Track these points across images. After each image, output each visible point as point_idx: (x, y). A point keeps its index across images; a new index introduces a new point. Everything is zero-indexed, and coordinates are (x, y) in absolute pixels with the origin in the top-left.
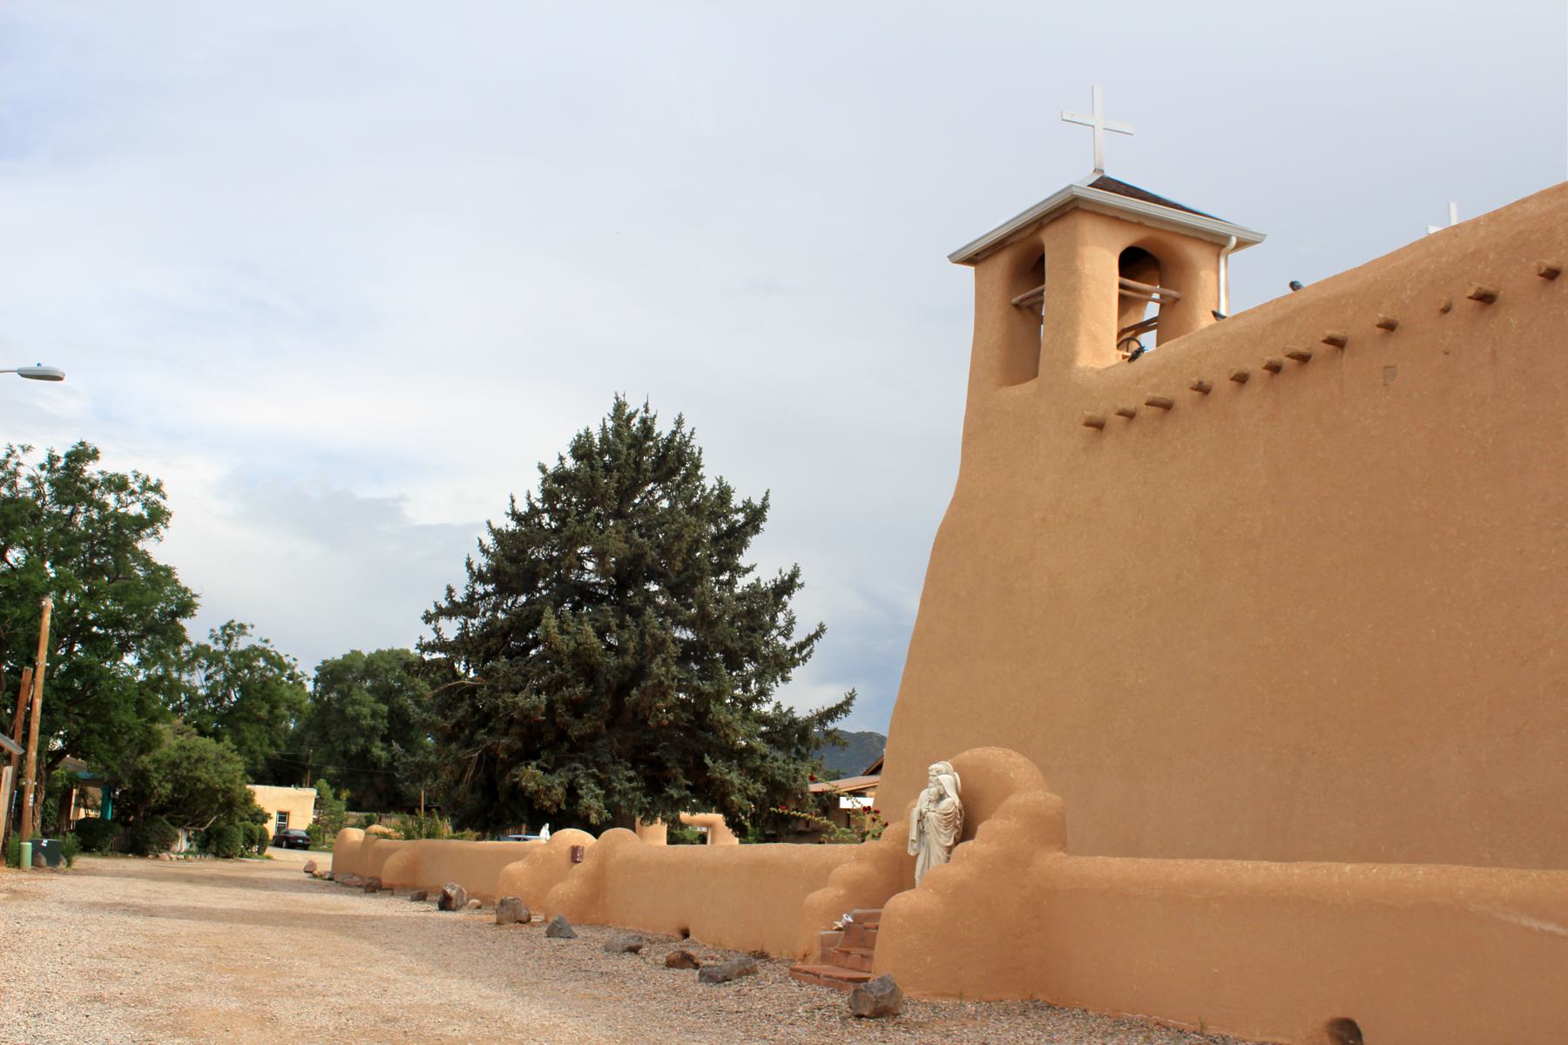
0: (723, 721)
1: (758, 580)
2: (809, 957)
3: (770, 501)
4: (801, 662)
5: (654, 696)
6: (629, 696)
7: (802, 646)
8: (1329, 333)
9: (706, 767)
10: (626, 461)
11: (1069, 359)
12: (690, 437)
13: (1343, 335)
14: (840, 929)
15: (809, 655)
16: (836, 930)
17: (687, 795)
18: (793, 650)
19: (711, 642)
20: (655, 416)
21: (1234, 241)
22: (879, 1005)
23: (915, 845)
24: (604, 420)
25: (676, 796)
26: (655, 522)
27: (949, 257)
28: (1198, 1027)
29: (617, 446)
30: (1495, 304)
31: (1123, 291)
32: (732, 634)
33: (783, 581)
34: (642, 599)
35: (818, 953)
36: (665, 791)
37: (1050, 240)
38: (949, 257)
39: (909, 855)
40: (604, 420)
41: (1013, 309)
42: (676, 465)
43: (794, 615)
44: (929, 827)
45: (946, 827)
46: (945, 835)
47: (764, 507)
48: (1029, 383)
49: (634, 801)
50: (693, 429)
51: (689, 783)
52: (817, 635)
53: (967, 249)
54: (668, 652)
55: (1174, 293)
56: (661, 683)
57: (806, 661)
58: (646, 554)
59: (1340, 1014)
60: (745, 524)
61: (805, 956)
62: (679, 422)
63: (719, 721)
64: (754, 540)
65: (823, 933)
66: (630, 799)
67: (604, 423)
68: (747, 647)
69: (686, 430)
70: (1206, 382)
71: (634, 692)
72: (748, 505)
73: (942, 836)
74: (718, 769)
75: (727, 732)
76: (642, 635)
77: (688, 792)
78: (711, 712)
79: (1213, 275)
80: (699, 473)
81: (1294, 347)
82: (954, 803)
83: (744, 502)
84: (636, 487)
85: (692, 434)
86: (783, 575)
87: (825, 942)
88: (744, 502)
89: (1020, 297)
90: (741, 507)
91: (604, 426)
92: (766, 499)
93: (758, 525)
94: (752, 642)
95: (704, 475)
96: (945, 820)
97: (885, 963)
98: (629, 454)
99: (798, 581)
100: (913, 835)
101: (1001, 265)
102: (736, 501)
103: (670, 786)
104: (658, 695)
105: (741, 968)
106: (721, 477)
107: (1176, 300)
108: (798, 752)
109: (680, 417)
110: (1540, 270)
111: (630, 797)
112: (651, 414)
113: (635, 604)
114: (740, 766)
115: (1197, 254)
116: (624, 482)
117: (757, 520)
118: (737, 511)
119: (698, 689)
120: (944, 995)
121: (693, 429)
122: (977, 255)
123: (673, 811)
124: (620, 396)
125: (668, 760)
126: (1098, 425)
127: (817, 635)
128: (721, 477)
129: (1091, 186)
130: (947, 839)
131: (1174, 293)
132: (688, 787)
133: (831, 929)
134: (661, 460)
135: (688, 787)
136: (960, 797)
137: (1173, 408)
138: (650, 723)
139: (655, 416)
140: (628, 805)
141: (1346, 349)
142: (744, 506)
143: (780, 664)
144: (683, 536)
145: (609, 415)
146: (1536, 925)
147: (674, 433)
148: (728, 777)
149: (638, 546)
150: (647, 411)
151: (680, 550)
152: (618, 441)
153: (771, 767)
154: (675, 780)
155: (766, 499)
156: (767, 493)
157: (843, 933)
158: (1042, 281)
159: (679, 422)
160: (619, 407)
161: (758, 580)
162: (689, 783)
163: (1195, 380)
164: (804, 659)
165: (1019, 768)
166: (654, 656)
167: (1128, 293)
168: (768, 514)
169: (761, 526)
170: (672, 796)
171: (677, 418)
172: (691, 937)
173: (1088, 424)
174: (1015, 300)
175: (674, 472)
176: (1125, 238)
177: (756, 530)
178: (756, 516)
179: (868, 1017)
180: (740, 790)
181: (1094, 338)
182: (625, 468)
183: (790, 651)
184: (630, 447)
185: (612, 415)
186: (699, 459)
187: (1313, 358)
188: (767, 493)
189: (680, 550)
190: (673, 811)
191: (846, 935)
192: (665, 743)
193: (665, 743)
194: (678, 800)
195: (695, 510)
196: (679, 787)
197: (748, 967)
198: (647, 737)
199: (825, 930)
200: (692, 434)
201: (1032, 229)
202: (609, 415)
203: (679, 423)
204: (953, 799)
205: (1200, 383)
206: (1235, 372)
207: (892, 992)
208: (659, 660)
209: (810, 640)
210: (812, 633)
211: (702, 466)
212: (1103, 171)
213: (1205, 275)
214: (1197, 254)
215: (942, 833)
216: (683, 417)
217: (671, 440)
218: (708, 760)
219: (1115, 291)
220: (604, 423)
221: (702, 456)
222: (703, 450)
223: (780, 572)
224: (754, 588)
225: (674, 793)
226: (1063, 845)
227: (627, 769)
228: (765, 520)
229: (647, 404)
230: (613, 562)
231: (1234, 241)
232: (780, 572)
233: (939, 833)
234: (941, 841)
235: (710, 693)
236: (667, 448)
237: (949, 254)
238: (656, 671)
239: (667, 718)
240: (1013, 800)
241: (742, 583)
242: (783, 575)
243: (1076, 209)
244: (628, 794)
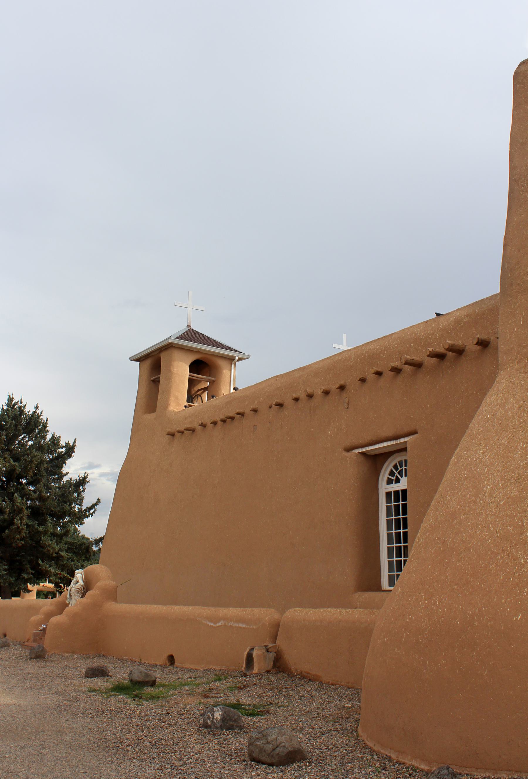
0: (47, 544)
1: (71, 479)
2: (29, 640)
3: (76, 444)
4: (90, 516)
5: (15, 533)
6: (5, 533)
7: (89, 509)
8: (238, 411)
9: (39, 565)
10: (10, 426)
11: (166, 406)
12: (41, 415)
13: (243, 411)
14: (41, 630)
15: (94, 512)
16: (40, 630)
17: (31, 577)
18: (85, 510)
19: (44, 509)
20: (26, 405)
21: (237, 358)
22: (37, 654)
23: (69, 600)
24: (3, 405)
25: (26, 577)
26: (22, 453)
27: (129, 358)
28: (139, 660)
29: (6, 419)
30: (283, 407)
31: (190, 377)
32: (54, 504)
33: (80, 480)
34: (15, 489)
35: (32, 639)
36: (22, 575)
37: (164, 356)
38: (129, 358)
39: (66, 603)
40: (3, 405)
41: (151, 382)
42: (34, 427)
43: (83, 496)
44: (72, 593)
45: (78, 593)
46: (77, 596)
47: (74, 446)
48: (152, 414)
49: (7, 580)
50: (42, 411)
51: (33, 572)
52: (97, 504)
53: (138, 355)
54: (24, 514)
55: (212, 379)
56: (18, 527)
57: (93, 515)
58: (16, 469)
59: (170, 654)
60: (65, 454)
61: (28, 640)
62: (37, 408)
63: (45, 544)
64: (68, 461)
65: (34, 631)
66: (5, 579)
67: (3, 407)
68: (61, 510)
69: (39, 412)
70: (204, 423)
71: (7, 531)
72: (68, 445)
73: (76, 596)
74: (44, 565)
75: (49, 549)
76: (13, 506)
77: (32, 576)
78: (42, 540)
79: (229, 372)
80: (47, 429)
81: (228, 414)
82: (81, 584)
83: (66, 443)
84: (16, 437)
85: (41, 413)
86: (80, 477)
87: (35, 635)
88: (66, 443)
89: (154, 378)
90: (65, 445)
91: (3, 408)
92: (74, 443)
93: (71, 454)
94: (63, 508)
95: (49, 430)
96: (77, 590)
97: (47, 642)
98: (12, 423)
99: (87, 480)
100: (68, 596)
101: (148, 363)
102: (63, 443)
103: (24, 573)
104: (17, 532)
105: (3, 644)
106: (54, 433)
107: (214, 381)
108: (86, 557)
109: (37, 405)
110: (292, 398)
111: (5, 578)
112: (24, 404)
113: (11, 491)
114: (57, 564)
115: (222, 363)
116: (9, 435)
117: (71, 452)
118: (62, 447)
119: (37, 530)
120: (67, 652)
121: (42, 411)
122: (140, 358)
123: (24, 584)
124: (11, 395)
125: (24, 561)
126: (172, 435)
127: (97, 504)
128: (54, 433)
129: (176, 338)
130: (78, 597)
131: (212, 379)
132: (32, 574)
133: (38, 630)
134: (28, 424)
135: (32, 574)
136: (83, 582)
137: (195, 431)
138: (13, 545)
139: (26, 405)
140: (4, 582)
141: (244, 417)
142: (66, 445)
143: (80, 517)
144: (33, 461)
145: (5, 403)
146: (236, 625)
147: (34, 412)
148: (49, 569)
149: (12, 465)
150: (21, 403)
151: (31, 468)
152: (7, 417)
153: (71, 564)
154: (27, 570)
155: (74, 443)
156: (75, 440)
157: (42, 631)
158: (160, 374)
159: (37, 408)
160: (10, 400)
161: (71, 479)
162: (33, 572)
163: (200, 422)
164: (92, 514)
165: (103, 572)
166: (17, 515)
167: (192, 377)
168: (76, 449)
169: (73, 455)
170: (24, 577)
171: (36, 406)
172: (7, 637)
173: (168, 434)
174: (152, 379)
175: (33, 430)
176: (192, 358)
177: (70, 456)
178: (70, 450)
179: (34, 658)
180: (55, 575)
181: (177, 398)
182: (10, 429)
183: (84, 511)
184: (13, 419)
185: (7, 403)
186: (46, 423)
187: (235, 418)
188: (75, 440)
189: (31, 468)
190: (24, 584)
191: (43, 632)
192: (23, 553)
193: (23, 553)
194: (27, 579)
195: (41, 448)
196: (28, 573)
197: (5, 644)
198: (15, 551)
199: (35, 630)
200: (41, 413)
201: (158, 352)
202: (5, 403)
203: (36, 408)
204: (81, 583)
205: (202, 423)
206: (212, 421)
207: (42, 650)
208: (18, 517)
209: (93, 506)
210: (94, 503)
211: (48, 427)
212: (191, 326)
213: (226, 372)
214: (222, 363)
215: (76, 595)
216: (38, 405)
217: (32, 416)
218: (40, 562)
219: (188, 377)
220: (3, 407)
221: (48, 422)
222: (48, 419)
223: (79, 476)
224: (69, 482)
225: (25, 576)
226: (115, 600)
227: (5, 565)
228: (74, 452)
229: (21, 400)
230: (4, 471)
231: (237, 358)
232: (79, 476)
233: (75, 595)
234: (76, 598)
235: (42, 531)
236: (30, 419)
237: (129, 357)
238: (16, 522)
239: (21, 543)
240: (99, 584)
241: (65, 479)
242: (80, 477)
243: (172, 346)
244: (4, 576)
